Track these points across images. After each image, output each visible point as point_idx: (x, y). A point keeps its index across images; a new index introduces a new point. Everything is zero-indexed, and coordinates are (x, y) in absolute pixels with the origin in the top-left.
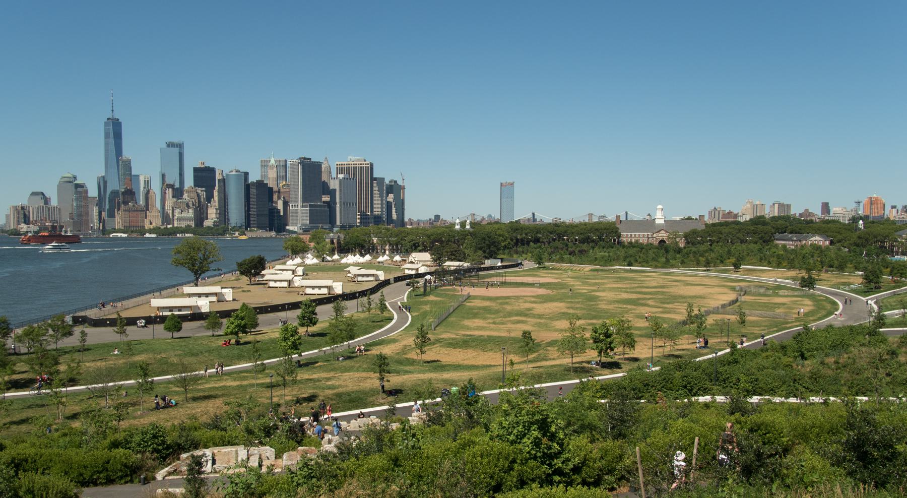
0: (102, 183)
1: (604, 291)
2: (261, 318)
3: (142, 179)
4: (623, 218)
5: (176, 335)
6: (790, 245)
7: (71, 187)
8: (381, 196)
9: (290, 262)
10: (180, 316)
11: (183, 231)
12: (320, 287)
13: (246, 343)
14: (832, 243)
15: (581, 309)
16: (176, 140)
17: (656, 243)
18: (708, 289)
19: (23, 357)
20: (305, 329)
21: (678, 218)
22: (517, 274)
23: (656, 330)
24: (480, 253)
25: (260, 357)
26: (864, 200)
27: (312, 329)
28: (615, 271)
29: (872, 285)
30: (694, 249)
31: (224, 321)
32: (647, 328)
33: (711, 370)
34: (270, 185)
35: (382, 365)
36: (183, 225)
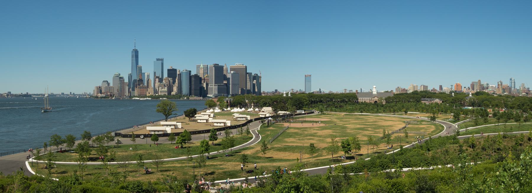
0: (130, 77)
1: (349, 124)
2: (193, 136)
3: (146, 74)
4: (359, 91)
5: (156, 142)
6: (427, 103)
7: (118, 78)
8: (250, 81)
9: (208, 111)
10: (158, 134)
11: (162, 97)
12: (220, 123)
13: (185, 147)
14: (443, 102)
15: (339, 132)
16: (160, 58)
17: (373, 102)
18: (393, 122)
19: (95, 149)
20: (212, 142)
21: (383, 91)
22: (311, 117)
23: (371, 142)
24: (294, 107)
25: (190, 154)
26: (454, 85)
27: (215, 142)
28: (355, 115)
29: (457, 119)
30: (389, 105)
31: (176, 137)
32: (366, 141)
33: (392, 158)
34: (200, 76)
35: (245, 159)
36: (163, 94)
